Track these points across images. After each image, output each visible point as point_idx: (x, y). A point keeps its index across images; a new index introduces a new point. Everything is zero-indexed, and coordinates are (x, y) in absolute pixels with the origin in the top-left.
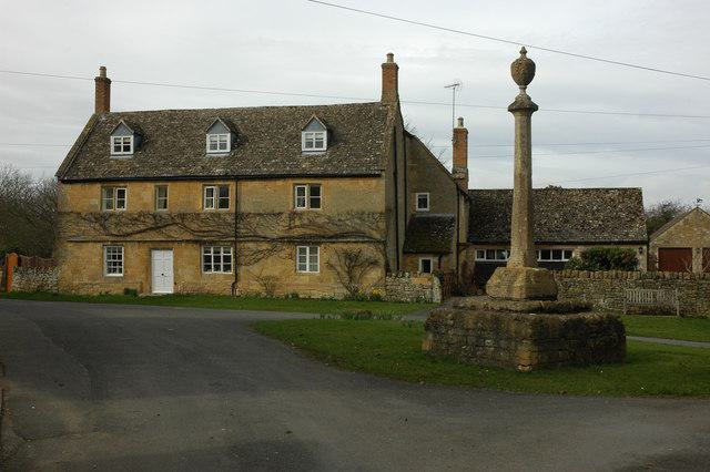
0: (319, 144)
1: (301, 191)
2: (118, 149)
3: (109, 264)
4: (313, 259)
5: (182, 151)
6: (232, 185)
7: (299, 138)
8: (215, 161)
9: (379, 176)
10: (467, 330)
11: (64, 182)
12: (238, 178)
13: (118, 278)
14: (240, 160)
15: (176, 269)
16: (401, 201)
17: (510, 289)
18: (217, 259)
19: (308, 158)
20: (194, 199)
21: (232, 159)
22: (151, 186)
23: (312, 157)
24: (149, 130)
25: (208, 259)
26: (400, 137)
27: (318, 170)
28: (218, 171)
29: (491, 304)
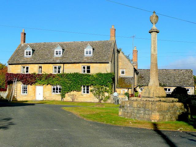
0: (90, 53)
1: (56, 68)
2: (87, 53)
3: (23, 90)
4: (11, 98)
5: (47, 55)
6: (62, 65)
7: (84, 51)
8: (57, 58)
9: (108, 63)
10: (134, 107)
11: (9, 64)
12: (64, 63)
13: (25, 95)
14: (65, 58)
15: (44, 92)
16: (116, 71)
17: (149, 93)
18: (57, 89)
19: (86, 57)
20: (49, 69)
21: (63, 57)
22: (37, 66)
23: (88, 57)
24: (65, 47)
25: (54, 89)
26: (116, 51)
27: (89, 61)
28: (58, 61)
29: (143, 99)
